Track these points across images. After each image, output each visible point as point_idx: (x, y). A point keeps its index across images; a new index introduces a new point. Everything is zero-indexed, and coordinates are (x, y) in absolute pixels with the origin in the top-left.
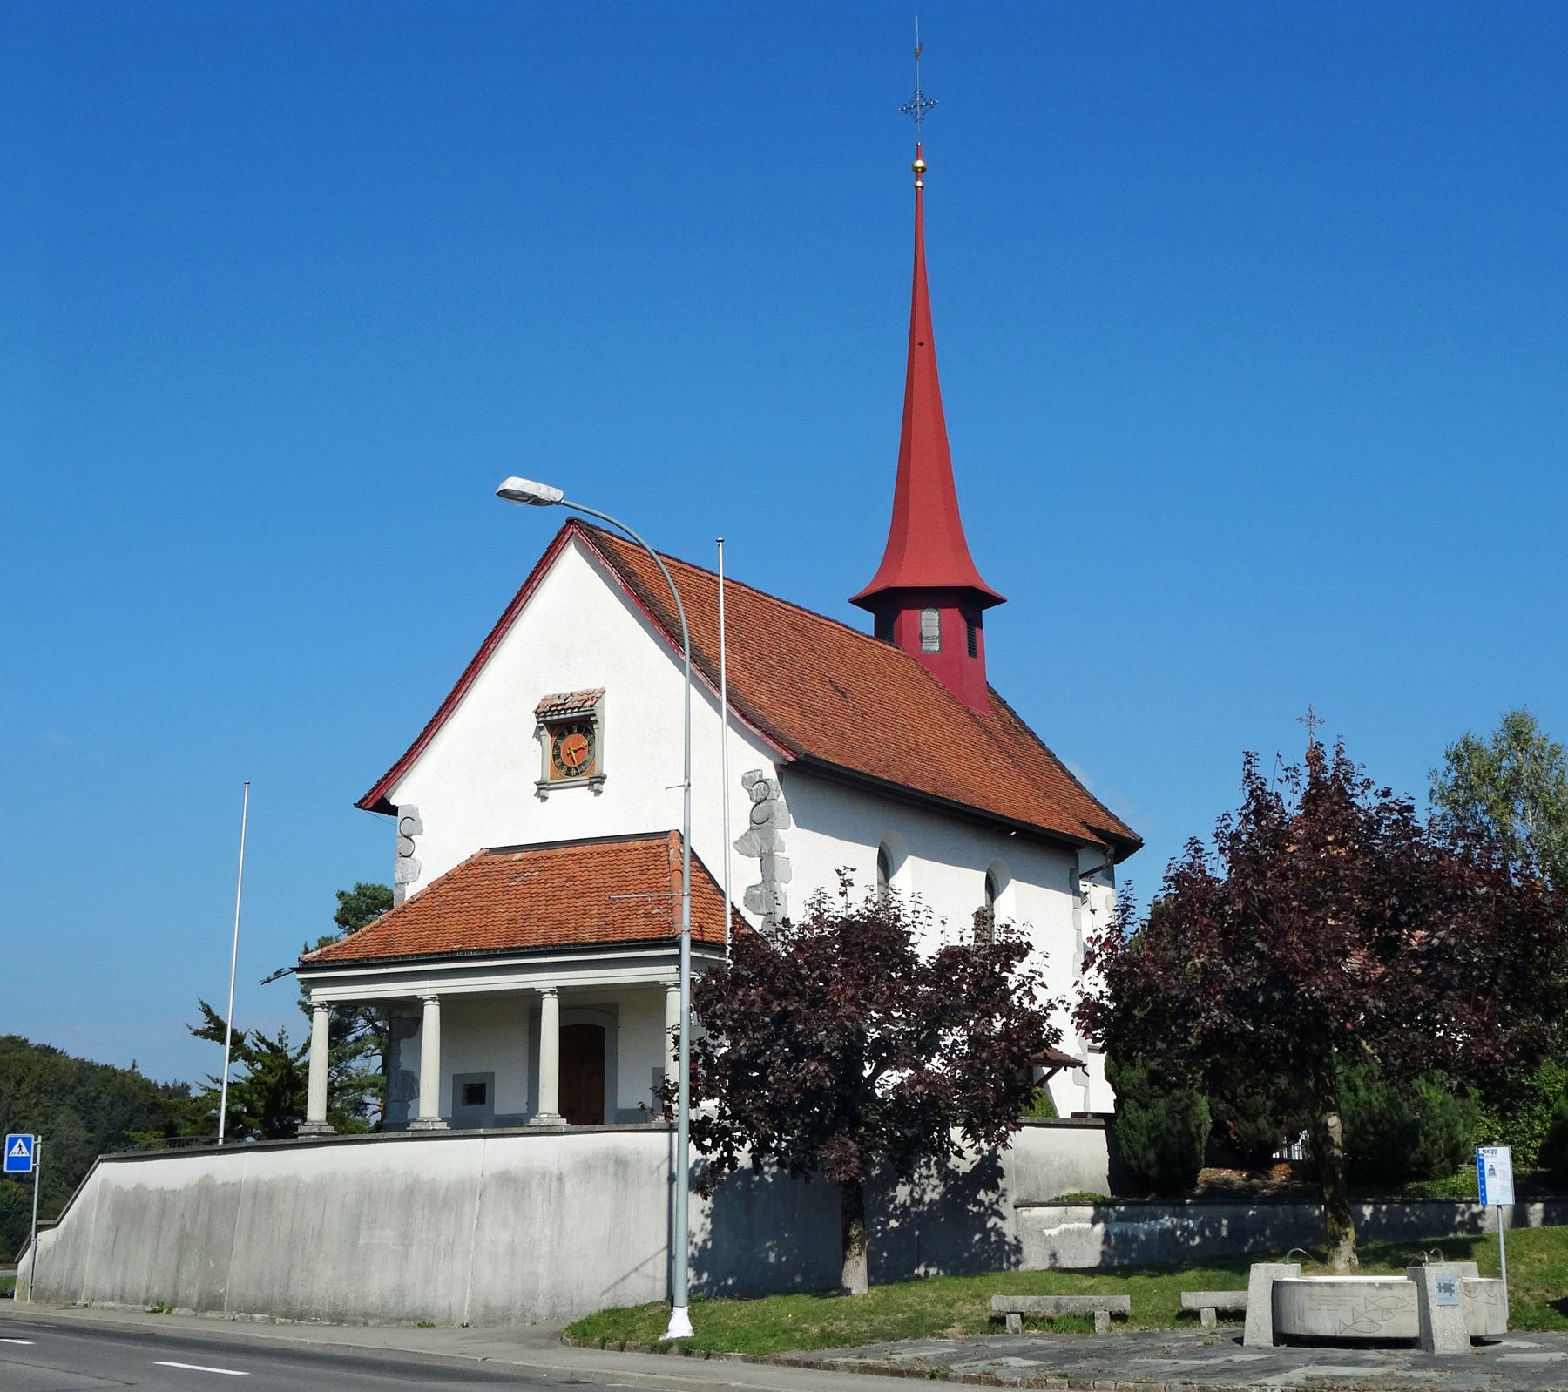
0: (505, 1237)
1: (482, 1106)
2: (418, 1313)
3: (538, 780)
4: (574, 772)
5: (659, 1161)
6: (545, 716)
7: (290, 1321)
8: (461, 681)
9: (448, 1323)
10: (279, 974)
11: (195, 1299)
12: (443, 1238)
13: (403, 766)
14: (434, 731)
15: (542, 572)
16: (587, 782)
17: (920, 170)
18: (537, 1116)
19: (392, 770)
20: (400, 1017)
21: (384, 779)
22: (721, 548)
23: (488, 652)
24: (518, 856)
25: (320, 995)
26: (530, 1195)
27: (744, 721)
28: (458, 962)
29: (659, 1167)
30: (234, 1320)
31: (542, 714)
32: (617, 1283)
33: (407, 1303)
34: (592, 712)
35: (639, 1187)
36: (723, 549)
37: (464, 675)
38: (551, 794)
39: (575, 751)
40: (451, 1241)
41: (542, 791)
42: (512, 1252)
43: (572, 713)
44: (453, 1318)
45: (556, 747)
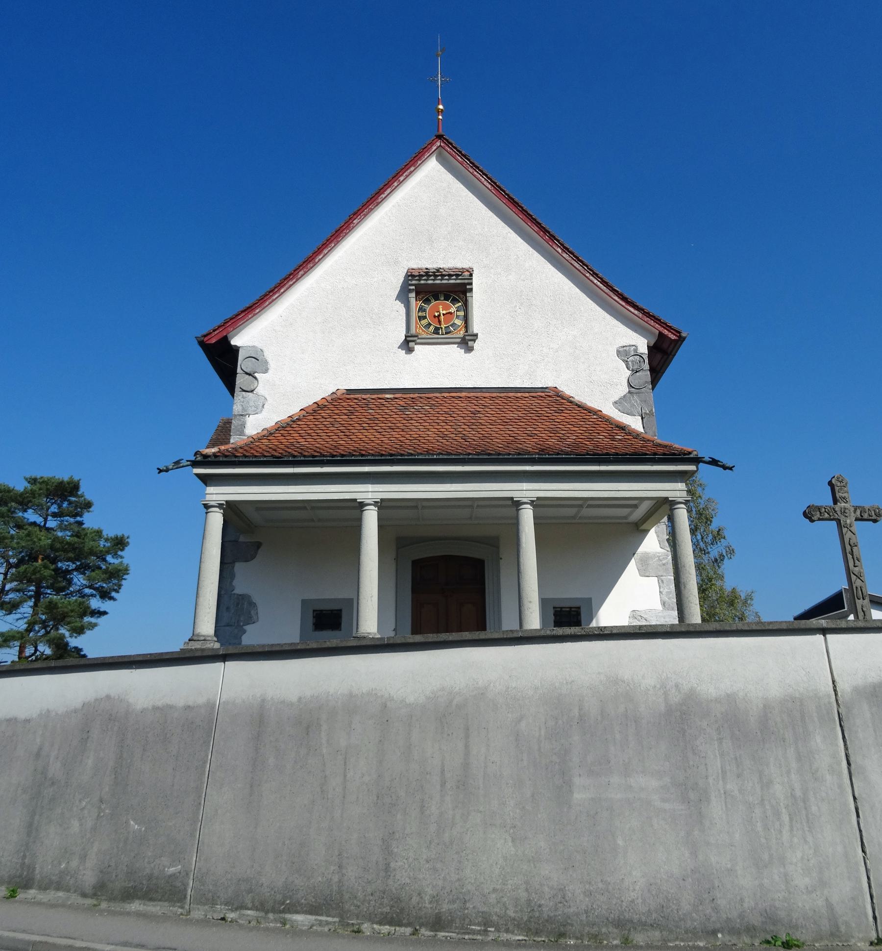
2: (756, 920)
6: (419, 280)
7: (408, 930)
10: (177, 464)
11: (89, 877)
12: (779, 790)
13: (254, 309)
14: (291, 283)
15: (409, 171)
16: (459, 340)
17: (440, 110)
20: (236, 541)
21: (231, 319)
25: (218, 494)
28: (273, 499)
30: (223, 919)
33: (722, 902)
34: (469, 281)
39: (443, 314)
40: (798, 793)
44: (843, 929)
45: (421, 309)
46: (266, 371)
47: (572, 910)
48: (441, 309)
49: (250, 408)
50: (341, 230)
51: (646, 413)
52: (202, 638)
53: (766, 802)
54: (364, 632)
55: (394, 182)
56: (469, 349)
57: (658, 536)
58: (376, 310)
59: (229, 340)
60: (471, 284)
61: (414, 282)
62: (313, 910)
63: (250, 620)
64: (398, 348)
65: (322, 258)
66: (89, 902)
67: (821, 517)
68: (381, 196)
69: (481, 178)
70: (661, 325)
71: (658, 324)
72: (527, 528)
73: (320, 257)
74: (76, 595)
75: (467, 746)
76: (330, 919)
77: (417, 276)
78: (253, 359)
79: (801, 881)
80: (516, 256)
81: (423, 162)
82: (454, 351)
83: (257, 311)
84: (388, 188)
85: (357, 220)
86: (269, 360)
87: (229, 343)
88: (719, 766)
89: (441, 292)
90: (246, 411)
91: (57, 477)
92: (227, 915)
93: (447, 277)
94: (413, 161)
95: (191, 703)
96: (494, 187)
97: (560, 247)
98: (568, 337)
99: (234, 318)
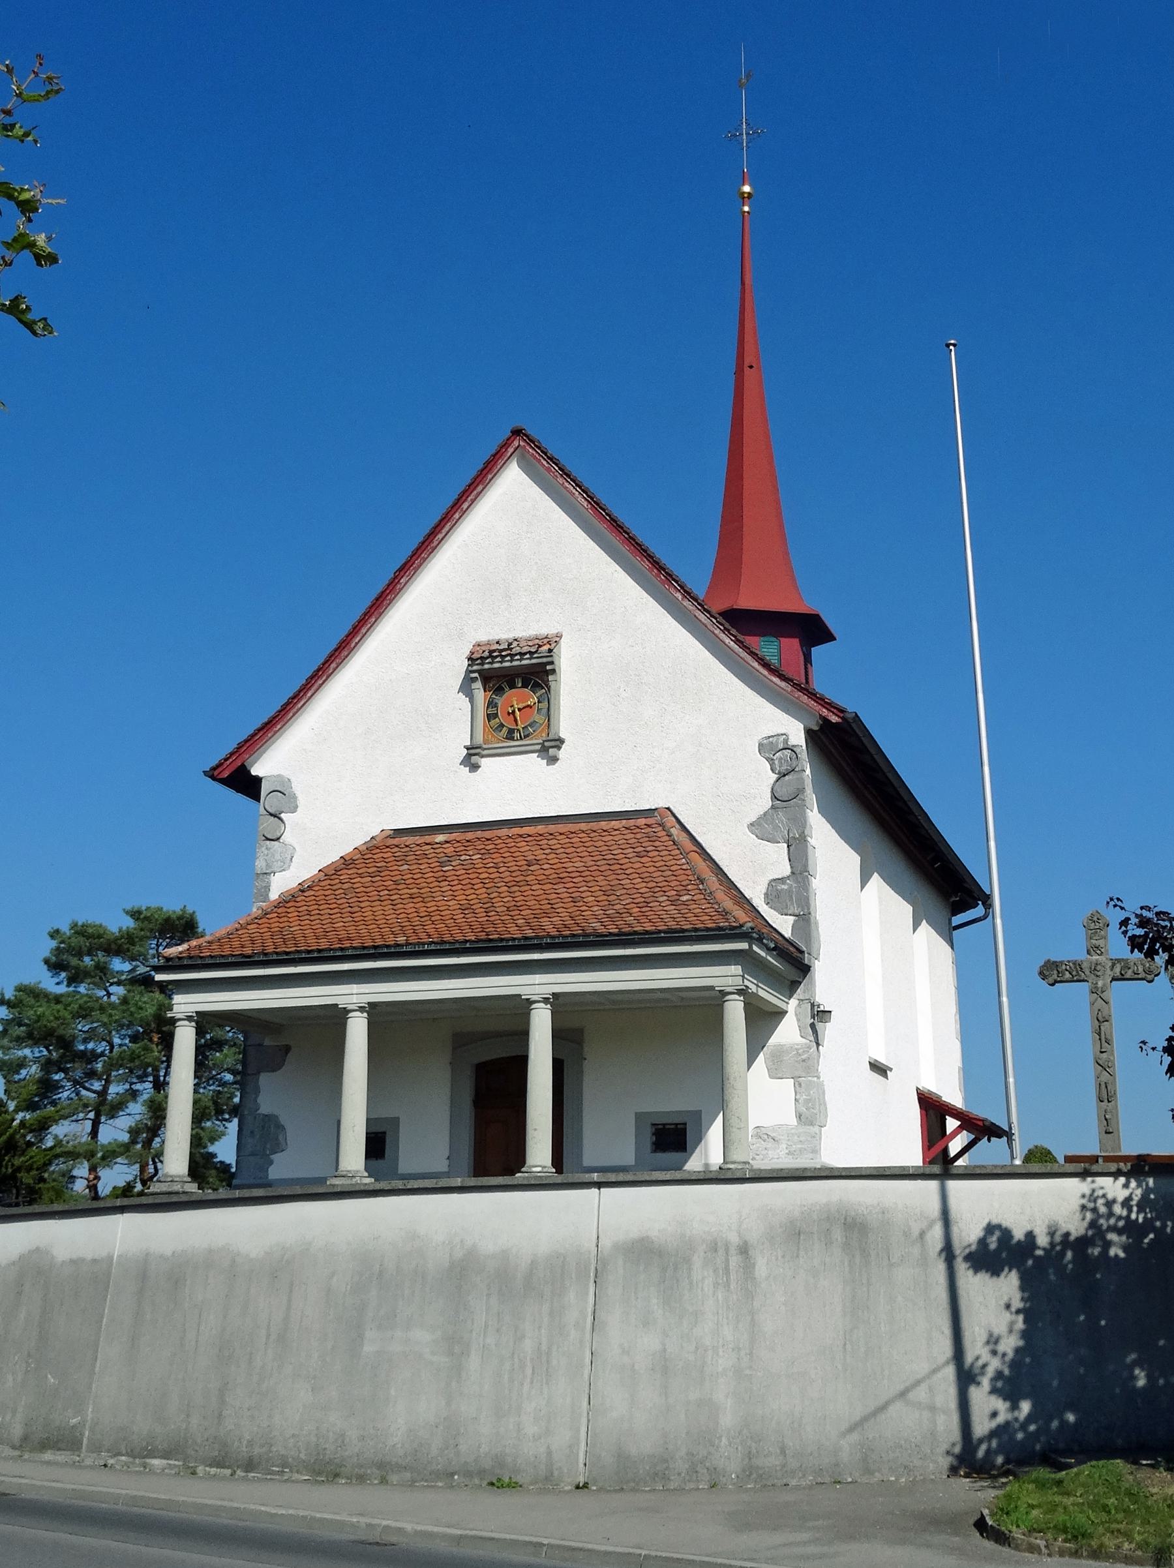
0: (649, 1342)
1: (380, 1161)
3: (468, 743)
4: (516, 735)
5: (924, 1225)
6: (482, 664)
7: (228, 1472)
8: (359, 622)
9: (548, 1482)
11: (17, 1431)
12: (528, 1345)
15: (475, 492)
16: (538, 747)
17: (746, 195)
18: (523, 1169)
19: (259, 730)
20: (260, 1045)
21: (246, 741)
22: (953, 353)
23: (398, 586)
24: (440, 838)
26: (689, 1276)
27: (765, 672)
29: (922, 1234)
30: (105, 1466)
31: (479, 661)
32: (865, 1419)
33: (463, 1448)
34: (549, 659)
35: (891, 1265)
36: (955, 354)
37: (365, 614)
38: (485, 762)
39: (519, 710)
40: (544, 1347)
41: (473, 758)
42: (663, 1366)
43: (520, 660)
44: (556, 1473)
45: (491, 704)
46: (294, 810)
47: (347, 1454)
48: (515, 703)
49: (275, 863)
50: (384, 596)
51: (794, 838)
52: (170, 1179)
53: (516, 1356)
54: (345, 1169)
55: (455, 513)
56: (553, 760)
57: (798, 1020)
58: (433, 710)
59: (248, 768)
60: (552, 663)
61: (475, 668)
62: (166, 1455)
63: (278, 1148)
64: (460, 764)
65: (359, 641)
66: (17, 1453)
67: (1059, 979)
68: (437, 538)
69: (574, 491)
70: (817, 702)
71: (814, 701)
72: (537, 1034)
73: (358, 639)
74: (214, 1083)
75: (289, 1301)
76: (176, 1463)
77: (477, 659)
78: (279, 794)
79: (531, 1429)
80: (623, 609)
81: (495, 474)
82: (533, 762)
83: (279, 727)
84: (447, 522)
85: (404, 577)
86: (298, 794)
87: (249, 772)
88: (484, 1320)
89: (518, 676)
90: (270, 867)
91: (164, 909)
92: (108, 1461)
93: (518, 657)
94: (480, 478)
95: (96, 1257)
96: (591, 504)
97: (679, 591)
98: (691, 729)
99: (250, 740)
